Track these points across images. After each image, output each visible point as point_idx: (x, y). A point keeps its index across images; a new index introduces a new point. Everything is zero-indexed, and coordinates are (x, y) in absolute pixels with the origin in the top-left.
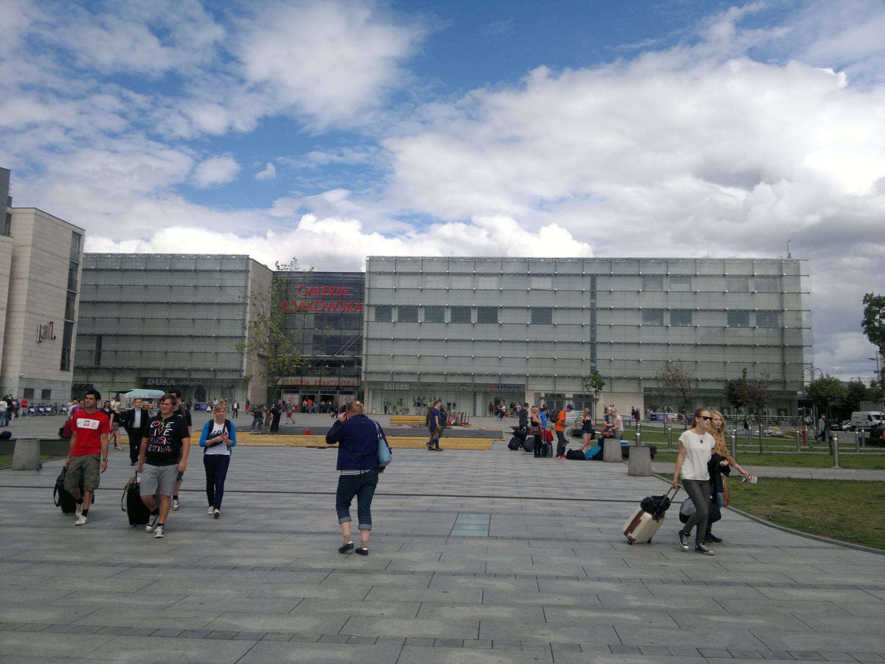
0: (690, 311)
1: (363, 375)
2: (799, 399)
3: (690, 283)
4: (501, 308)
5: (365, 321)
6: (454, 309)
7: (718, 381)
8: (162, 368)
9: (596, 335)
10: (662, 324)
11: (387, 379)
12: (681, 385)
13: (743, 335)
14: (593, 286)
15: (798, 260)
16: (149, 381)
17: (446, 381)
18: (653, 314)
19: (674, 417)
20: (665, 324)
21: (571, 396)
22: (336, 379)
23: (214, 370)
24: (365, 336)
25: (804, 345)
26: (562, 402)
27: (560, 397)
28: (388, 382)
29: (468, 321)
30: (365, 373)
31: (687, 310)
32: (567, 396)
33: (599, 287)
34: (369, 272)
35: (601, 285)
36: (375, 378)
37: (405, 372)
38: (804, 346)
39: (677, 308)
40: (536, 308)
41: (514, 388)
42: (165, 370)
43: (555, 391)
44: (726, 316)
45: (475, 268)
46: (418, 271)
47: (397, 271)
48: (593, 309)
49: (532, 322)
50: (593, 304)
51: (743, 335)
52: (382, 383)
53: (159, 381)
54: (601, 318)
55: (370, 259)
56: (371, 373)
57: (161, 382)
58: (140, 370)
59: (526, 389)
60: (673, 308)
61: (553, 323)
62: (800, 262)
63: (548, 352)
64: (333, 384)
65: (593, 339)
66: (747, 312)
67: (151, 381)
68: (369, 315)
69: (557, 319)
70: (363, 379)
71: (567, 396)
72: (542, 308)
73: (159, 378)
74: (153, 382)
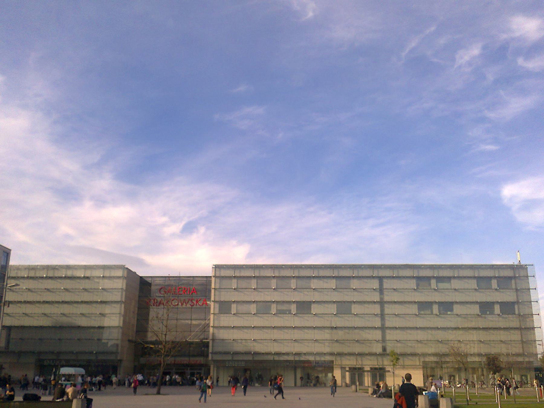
0: (350, 302)
1: (210, 355)
2: (535, 367)
3: (451, 283)
4: (314, 302)
5: (212, 314)
6: (440, 304)
7: (480, 355)
8: (75, 352)
9: (385, 322)
10: (432, 314)
11: (230, 358)
12: (461, 359)
13: (492, 321)
14: (381, 284)
15: (526, 265)
16: (45, 362)
17: (253, 359)
18: (424, 306)
19: (446, 383)
20: (434, 312)
21: (369, 369)
22: (187, 359)
23: (77, 353)
24: (211, 324)
25: (535, 327)
26: (362, 374)
27: (194, 373)
28: (229, 361)
29: (492, 313)
30: (212, 353)
31: (430, 302)
32: (366, 369)
33: (385, 286)
34: (215, 276)
35: (387, 284)
36: (218, 357)
37: (242, 352)
38: (535, 328)
39: (443, 300)
40: (442, 303)
41: (493, 361)
42: (59, 353)
43: (357, 365)
44: (416, 306)
45: (294, 273)
46: (231, 275)
47: (236, 275)
48: (382, 303)
49: (219, 312)
50: (382, 299)
51: (492, 321)
52: (224, 361)
53: (53, 362)
54: (388, 309)
55: (215, 266)
56: (216, 353)
57: (54, 362)
58: (40, 353)
59: (334, 363)
60: (419, 301)
61: (353, 312)
62: (527, 266)
63: (340, 335)
64: (185, 362)
65: (383, 325)
66: (493, 303)
67: (47, 362)
68: (213, 307)
69: (315, 309)
70: (210, 358)
71: (366, 369)
72: (304, 302)
73: (53, 360)
74: (48, 362)
